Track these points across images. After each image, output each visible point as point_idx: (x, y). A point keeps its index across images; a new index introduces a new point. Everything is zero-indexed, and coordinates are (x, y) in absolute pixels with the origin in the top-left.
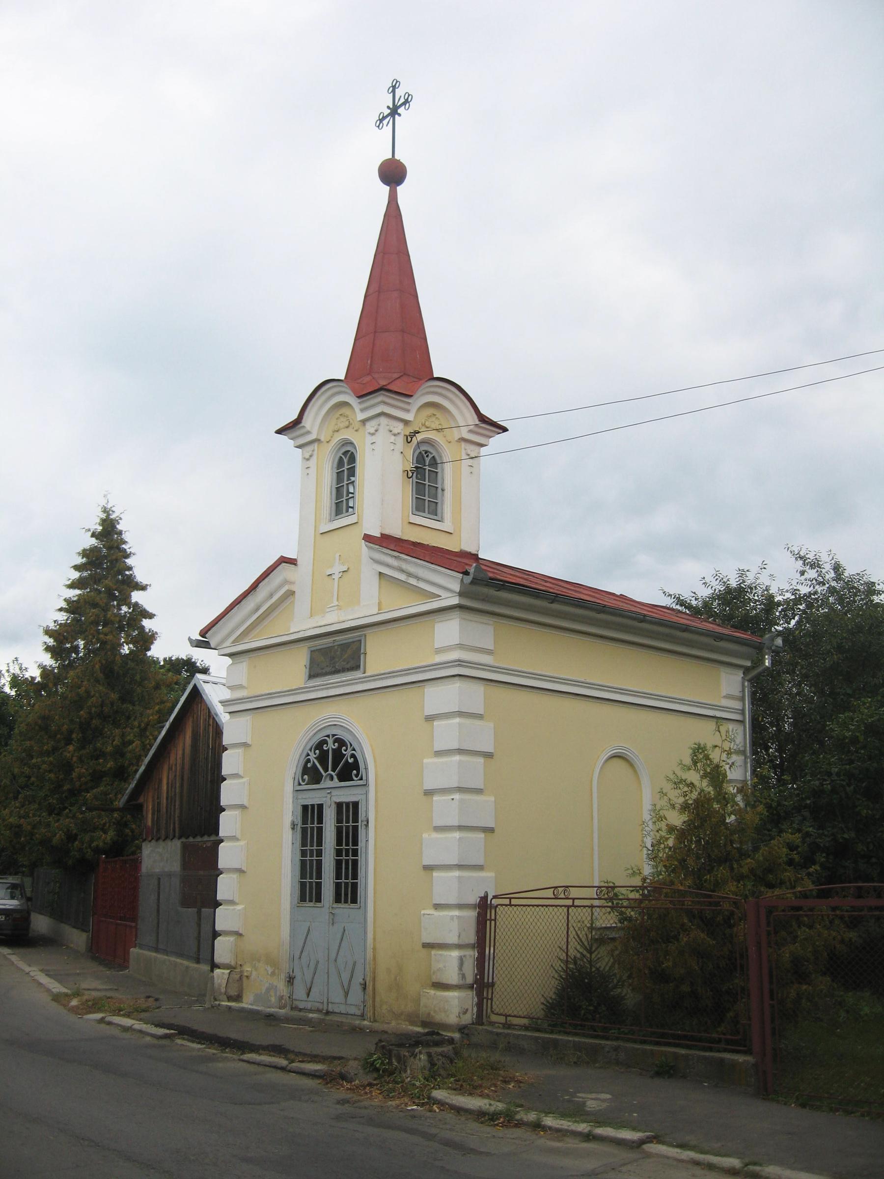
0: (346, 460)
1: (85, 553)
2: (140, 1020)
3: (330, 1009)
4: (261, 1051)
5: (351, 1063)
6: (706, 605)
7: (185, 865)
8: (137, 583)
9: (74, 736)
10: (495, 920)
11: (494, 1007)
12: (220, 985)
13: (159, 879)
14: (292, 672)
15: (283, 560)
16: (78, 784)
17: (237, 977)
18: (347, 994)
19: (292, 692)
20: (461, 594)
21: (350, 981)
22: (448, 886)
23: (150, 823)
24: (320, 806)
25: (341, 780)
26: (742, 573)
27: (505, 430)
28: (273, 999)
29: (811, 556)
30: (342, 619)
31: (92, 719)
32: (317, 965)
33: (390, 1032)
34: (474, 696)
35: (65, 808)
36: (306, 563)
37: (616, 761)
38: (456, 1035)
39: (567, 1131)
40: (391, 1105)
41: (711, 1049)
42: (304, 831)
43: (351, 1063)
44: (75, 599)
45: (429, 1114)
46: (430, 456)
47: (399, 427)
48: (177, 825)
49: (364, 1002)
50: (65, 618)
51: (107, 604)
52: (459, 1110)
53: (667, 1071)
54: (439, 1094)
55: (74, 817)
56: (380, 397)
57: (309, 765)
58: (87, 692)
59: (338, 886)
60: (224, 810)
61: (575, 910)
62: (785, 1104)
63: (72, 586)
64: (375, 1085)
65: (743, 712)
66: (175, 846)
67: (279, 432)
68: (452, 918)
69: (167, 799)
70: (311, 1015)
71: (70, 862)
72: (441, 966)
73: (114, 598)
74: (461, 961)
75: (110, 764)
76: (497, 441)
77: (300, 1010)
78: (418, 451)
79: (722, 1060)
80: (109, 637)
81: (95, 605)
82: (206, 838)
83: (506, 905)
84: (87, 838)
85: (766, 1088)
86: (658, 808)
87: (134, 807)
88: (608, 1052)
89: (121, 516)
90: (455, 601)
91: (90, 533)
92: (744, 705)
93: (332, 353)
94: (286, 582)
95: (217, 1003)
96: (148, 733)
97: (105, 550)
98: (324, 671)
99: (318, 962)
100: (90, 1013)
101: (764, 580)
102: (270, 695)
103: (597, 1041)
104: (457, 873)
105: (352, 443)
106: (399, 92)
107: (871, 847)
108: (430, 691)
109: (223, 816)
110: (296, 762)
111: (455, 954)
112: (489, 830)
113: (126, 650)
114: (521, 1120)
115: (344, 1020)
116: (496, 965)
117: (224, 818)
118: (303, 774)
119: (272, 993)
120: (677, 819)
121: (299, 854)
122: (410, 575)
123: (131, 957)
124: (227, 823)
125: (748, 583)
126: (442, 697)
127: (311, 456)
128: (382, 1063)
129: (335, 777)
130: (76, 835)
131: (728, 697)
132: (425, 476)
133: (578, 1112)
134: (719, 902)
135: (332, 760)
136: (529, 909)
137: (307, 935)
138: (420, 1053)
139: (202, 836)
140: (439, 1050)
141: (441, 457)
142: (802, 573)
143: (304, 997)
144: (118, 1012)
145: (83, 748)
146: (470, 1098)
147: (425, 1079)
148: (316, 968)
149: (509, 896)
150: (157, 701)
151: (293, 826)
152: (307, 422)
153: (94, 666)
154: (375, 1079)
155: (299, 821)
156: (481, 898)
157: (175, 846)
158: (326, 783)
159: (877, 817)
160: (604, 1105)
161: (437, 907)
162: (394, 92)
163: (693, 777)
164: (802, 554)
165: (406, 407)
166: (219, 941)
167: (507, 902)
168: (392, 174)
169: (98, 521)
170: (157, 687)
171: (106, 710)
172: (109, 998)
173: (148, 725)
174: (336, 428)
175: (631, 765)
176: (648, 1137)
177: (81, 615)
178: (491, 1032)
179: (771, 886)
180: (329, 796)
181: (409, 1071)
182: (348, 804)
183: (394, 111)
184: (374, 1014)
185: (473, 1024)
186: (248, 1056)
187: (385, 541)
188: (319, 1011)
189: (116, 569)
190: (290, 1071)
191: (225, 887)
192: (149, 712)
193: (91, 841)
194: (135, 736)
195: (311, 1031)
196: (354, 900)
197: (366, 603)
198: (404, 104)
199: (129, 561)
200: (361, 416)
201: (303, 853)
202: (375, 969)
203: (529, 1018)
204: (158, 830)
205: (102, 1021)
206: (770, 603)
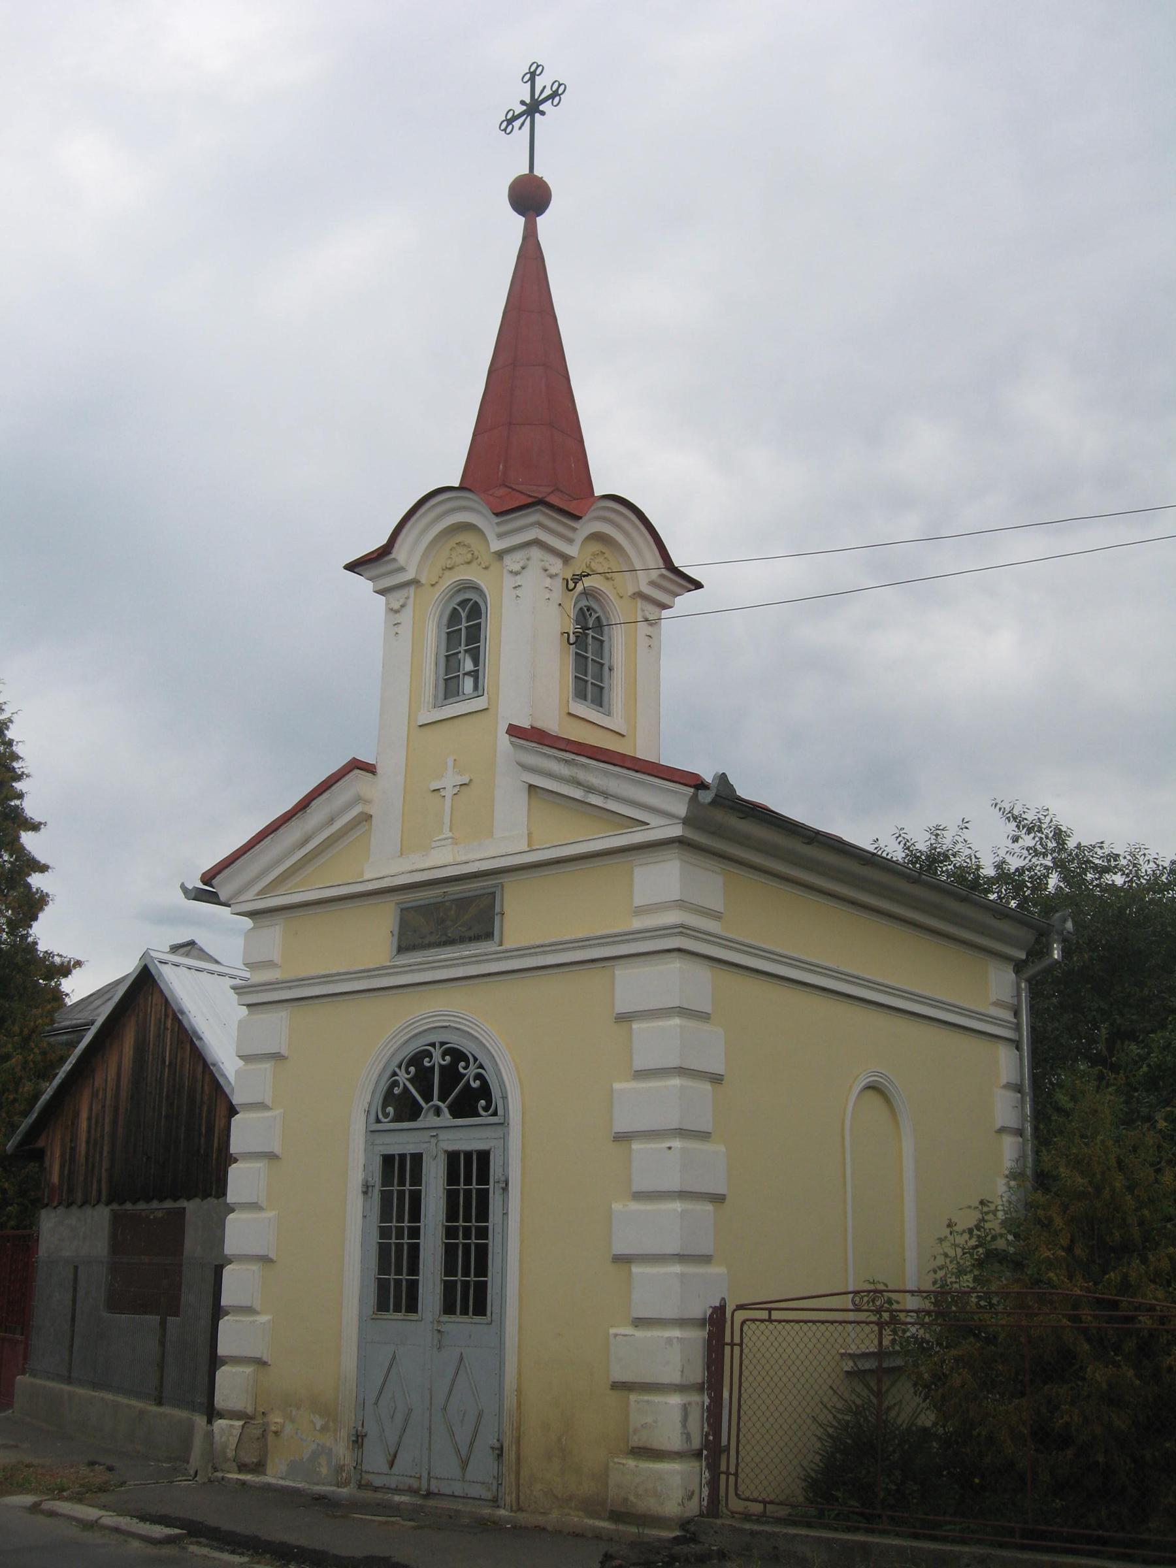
0: (464, 615)
2: (104, 1507)
3: (434, 1489)
7: (116, 1246)
11: (742, 1488)
13: (76, 1268)
14: (371, 940)
15: (356, 765)
17: (258, 1432)
18: (465, 1464)
19: (368, 973)
21: (472, 1444)
22: (667, 1291)
23: (55, 1179)
24: (417, 1158)
27: (698, 585)
28: (324, 1470)
29: (1030, 816)
30: (459, 859)
32: (409, 1414)
33: (549, 1528)
36: (392, 766)
37: (870, 1093)
42: (386, 1198)
46: (594, 616)
47: (556, 566)
48: (104, 1185)
49: (498, 1477)
56: (535, 516)
57: (396, 1091)
65: (1018, 1028)
66: (101, 1216)
67: (351, 567)
68: (669, 1341)
69: (88, 1142)
70: (397, 1498)
72: (649, 1420)
74: (685, 1408)
76: (686, 601)
77: (376, 1489)
82: (155, 1204)
83: (762, 1321)
90: (677, 831)
93: (441, 449)
94: (358, 799)
95: (220, 1474)
96: (32, 1045)
98: (426, 941)
102: (327, 978)
103: (947, 1547)
104: (677, 1269)
105: (476, 589)
106: (540, 82)
108: (622, 973)
111: (675, 1400)
112: (718, 1199)
118: (385, 1105)
119: (323, 1460)
121: (375, 1233)
122: (590, 789)
124: (242, 1180)
126: (636, 985)
127: (402, 606)
129: (446, 1110)
131: (998, 1004)
135: (445, 1081)
141: (608, 619)
142: (1016, 839)
143: (385, 1468)
144: (59, 1492)
148: (406, 1421)
149: (768, 1306)
151: (366, 1189)
152: (400, 553)
155: (377, 1179)
156: (715, 1309)
157: (101, 1216)
158: (427, 1120)
161: (639, 1322)
162: (532, 80)
164: (1016, 812)
165: (570, 534)
166: (222, 1374)
167: (764, 1315)
168: (530, 197)
172: (28, 1466)
173: (33, 1031)
174: (449, 563)
175: (887, 1100)
180: (434, 1141)
182: (468, 1155)
183: (533, 108)
184: (518, 1497)
185: (701, 1515)
192: (34, 1011)
195: (415, 1528)
196: (480, 1309)
197: (509, 832)
199: (18, 786)
200: (496, 545)
201: (384, 1233)
203: (792, 1506)
204: (71, 1191)
205: (35, 1508)
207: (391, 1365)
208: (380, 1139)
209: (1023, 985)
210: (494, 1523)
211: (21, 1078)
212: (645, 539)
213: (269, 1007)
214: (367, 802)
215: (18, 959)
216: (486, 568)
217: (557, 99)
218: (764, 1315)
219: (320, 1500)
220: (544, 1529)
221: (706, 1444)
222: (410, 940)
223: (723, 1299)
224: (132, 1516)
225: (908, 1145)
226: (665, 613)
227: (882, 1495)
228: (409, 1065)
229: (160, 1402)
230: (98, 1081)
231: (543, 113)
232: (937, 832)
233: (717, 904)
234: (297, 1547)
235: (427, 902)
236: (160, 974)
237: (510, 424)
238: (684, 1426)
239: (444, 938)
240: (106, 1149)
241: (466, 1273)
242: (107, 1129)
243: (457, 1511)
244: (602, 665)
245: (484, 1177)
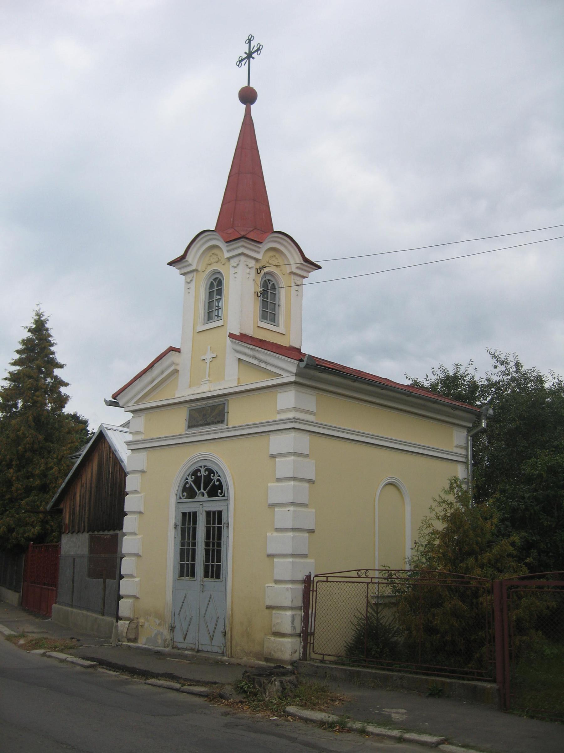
0: (215, 284)
1: (24, 342)
2: (71, 654)
4: (159, 678)
5: (227, 686)
6: (434, 387)
7: (92, 550)
8: (57, 363)
9: (14, 463)
10: (316, 591)
12: (122, 632)
13: (74, 559)
14: (177, 423)
15: (172, 349)
16: (15, 494)
17: (135, 626)
18: (212, 639)
20: (297, 375)
22: (284, 568)
23: (67, 521)
24: (195, 514)
25: (209, 496)
26: (457, 366)
27: (319, 267)
28: (160, 641)
29: (503, 357)
30: (212, 389)
31: (26, 451)
34: (303, 442)
35: (6, 510)
36: (186, 350)
38: (289, 667)
39: (384, 735)
40: (259, 717)
41: (463, 679)
42: (183, 530)
43: (227, 686)
44: (16, 372)
45: (286, 723)
46: (271, 283)
47: (252, 263)
48: (86, 524)
49: (224, 644)
50: (9, 385)
51: (38, 377)
52: (306, 720)
53: (436, 693)
54: (291, 709)
55: (13, 516)
57: (187, 486)
58: (24, 434)
59: (206, 567)
60: (126, 515)
61: (372, 585)
62: (520, 716)
63: (14, 364)
64: (244, 702)
65: (467, 456)
66: (85, 537)
67: (170, 264)
68: (287, 589)
69: (80, 505)
70: (186, 652)
71: (9, 546)
72: (279, 621)
73: (42, 372)
74: (293, 617)
75: (38, 482)
76: (315, 275)
77: (179, 649)
78: (264, 279)
79: (476, 687)
80: (40, 399)
81: (30, 377)
82: (106, 532)
83: (324, 581)
84: (21, 530)
85: (505, 706)
86: (428, 518)
87: (57, 511)
88: (396, 680)
89: (49, 318)
90: (293, 379)
91: (27, 330)
92: (467, 452)
94: (173, 363)
95: (120, 643)
96: (63, 462)
97: (37, 341)
98: (199, 424)
99: (192, 617)
100: (34, 649)
101: (471, 371)
102: (161, 439)
104: (291, 560)
105: (220, 273)
106: (253, 43)
107: (549, 546)
109: (126, 518)
110: (178, 483)
111: (289, 613)
112: (311, 531)
113: (49, 407)
114: (351, 727)
115: (210, 656)
116: (317, 621)
117: (127, 520)
119: (159, 637)
120: (440, 526)
122: (260, 361)
123: (53, 611)
124: (129, 523)
125: (460, 373)
126: (281, 443)
127: (191, 281)
128: (249, 687)
129: (206, 494)
130: (14, 528)
131: (457, 446)
132: (268, 296)
133: (387, 722)
134: (469, 582)
135: (205, 483)
136: (334, 584)
137: (184, 599)
138: (275, 680)
139: (104, 531)
140: (288, 679)
141: (278, 284)
142: (495, 367)
143: (182, 640)
144: (55, 649)
145: (19, 471)
146: (313, 712)
147: (279, 698)
148: (190, 621)
149: (326, 575)
150: (69, 441)
151: (176, 526)
153: (28, 417)
154: (244, 698)
155: (180, 522)
156: (307, 576)
157: (85, 537)
158: (199, 498)
159: (553, 526)
160: (404, 717)
161: (277, 582)
162: (249, 43)
163: (451, 498)
164: (496, 354)
166: (121, 602)
167: (325, 579)
168: (248, 96)
169: (33, 321)
170: (69, 432)
171: (36, 446)
172: (45, 639)
173: (63, 457)
174: (209, 262)
176: (441, 740)
177: (19, 383)
178: (313, 666)
179: (500, 571)
180: (201, 506)
181: (267, 693)
182: (214, 512)
183: (249, 56)
185: (300, 660)
186: (150, 681)
187: (242, 338)
188: (192, 649)
189: (44, 354)
190: (183, 692)
191: (127, 566)
192: (64, 448)
193: (24, 532)
194: (54, 464)
195: (189, 663)
196: (218, 576)
197: (230, 379)
198: (257, 51)
199: (52, 349)
200: (227, 255)
201: (183, 544)
202: (232, 622)
204: (73, 527)
205: (44, 655)
206: (474, 386)
207: (184, 599)
208: (181, 506)
209: (469, 438)
210: (222, 662)
211: (58, 477)
212: (295, 250)
213: (142, 450)
214: (177, 364)
215: (56, 425)
216: (223, 265)
217: (259, 52)
218: (325, 579)
219: (158, 653)
220: (240, 665)
221: (302, 631)
222: (192, 424)
223: (310, 572)
224: (79, 657)
225: (408, 508)
226: (305, 281)
227: (373, 653)
228: (192, 475)
229: (103, 614)
230: (84, 480)
231: (253, 58)
232: (457, 366)
233: (313, 408)
234: (139, 669)
235: (198, 407)
236: (107, 434)
237: (236, 200)
238: (293, 623)
239: (206, 422)
240: (87, 509)
241: (213, 561)
242: (87, 501)
243: (208, 658)
244: (275, 304)
245: (220, 522)
